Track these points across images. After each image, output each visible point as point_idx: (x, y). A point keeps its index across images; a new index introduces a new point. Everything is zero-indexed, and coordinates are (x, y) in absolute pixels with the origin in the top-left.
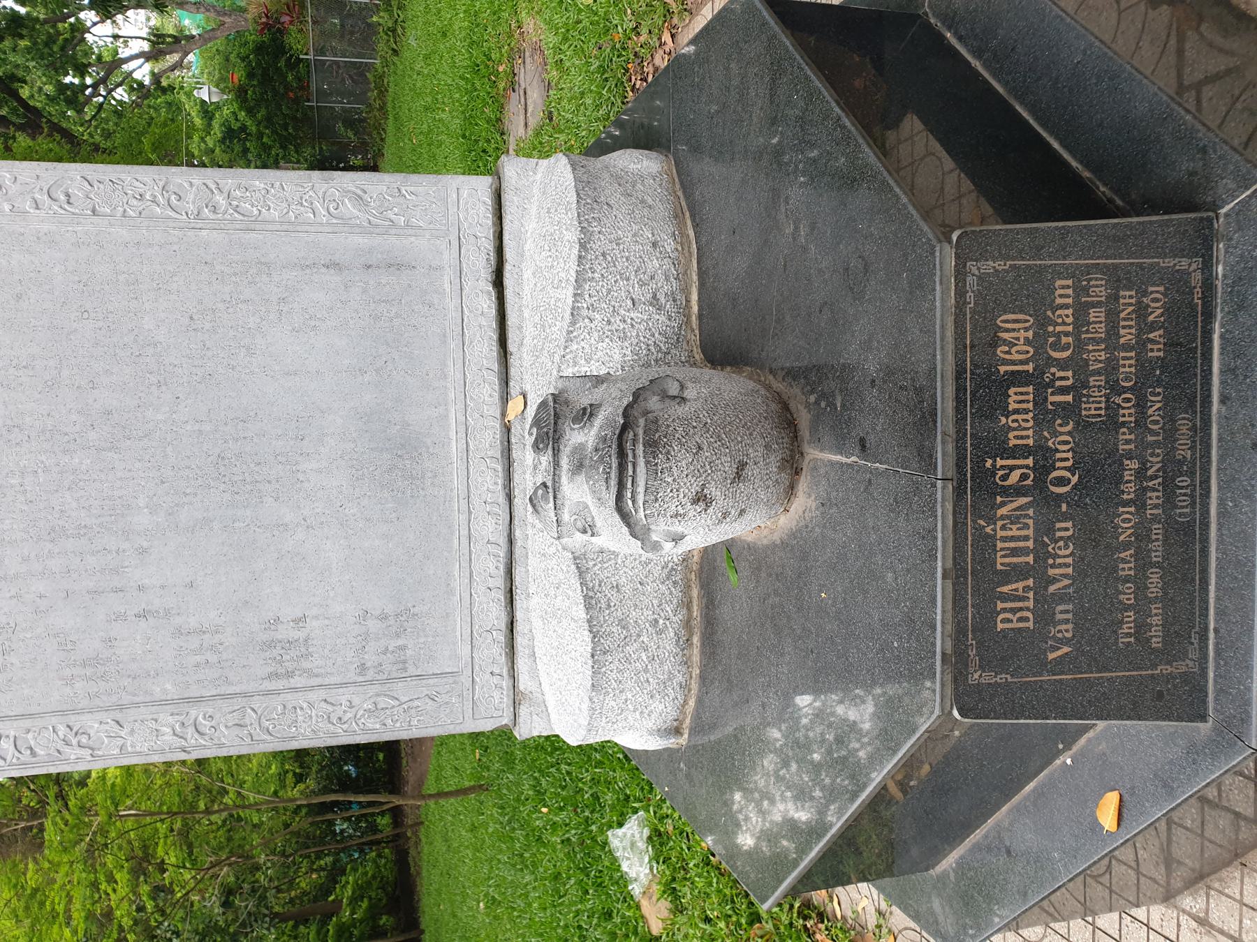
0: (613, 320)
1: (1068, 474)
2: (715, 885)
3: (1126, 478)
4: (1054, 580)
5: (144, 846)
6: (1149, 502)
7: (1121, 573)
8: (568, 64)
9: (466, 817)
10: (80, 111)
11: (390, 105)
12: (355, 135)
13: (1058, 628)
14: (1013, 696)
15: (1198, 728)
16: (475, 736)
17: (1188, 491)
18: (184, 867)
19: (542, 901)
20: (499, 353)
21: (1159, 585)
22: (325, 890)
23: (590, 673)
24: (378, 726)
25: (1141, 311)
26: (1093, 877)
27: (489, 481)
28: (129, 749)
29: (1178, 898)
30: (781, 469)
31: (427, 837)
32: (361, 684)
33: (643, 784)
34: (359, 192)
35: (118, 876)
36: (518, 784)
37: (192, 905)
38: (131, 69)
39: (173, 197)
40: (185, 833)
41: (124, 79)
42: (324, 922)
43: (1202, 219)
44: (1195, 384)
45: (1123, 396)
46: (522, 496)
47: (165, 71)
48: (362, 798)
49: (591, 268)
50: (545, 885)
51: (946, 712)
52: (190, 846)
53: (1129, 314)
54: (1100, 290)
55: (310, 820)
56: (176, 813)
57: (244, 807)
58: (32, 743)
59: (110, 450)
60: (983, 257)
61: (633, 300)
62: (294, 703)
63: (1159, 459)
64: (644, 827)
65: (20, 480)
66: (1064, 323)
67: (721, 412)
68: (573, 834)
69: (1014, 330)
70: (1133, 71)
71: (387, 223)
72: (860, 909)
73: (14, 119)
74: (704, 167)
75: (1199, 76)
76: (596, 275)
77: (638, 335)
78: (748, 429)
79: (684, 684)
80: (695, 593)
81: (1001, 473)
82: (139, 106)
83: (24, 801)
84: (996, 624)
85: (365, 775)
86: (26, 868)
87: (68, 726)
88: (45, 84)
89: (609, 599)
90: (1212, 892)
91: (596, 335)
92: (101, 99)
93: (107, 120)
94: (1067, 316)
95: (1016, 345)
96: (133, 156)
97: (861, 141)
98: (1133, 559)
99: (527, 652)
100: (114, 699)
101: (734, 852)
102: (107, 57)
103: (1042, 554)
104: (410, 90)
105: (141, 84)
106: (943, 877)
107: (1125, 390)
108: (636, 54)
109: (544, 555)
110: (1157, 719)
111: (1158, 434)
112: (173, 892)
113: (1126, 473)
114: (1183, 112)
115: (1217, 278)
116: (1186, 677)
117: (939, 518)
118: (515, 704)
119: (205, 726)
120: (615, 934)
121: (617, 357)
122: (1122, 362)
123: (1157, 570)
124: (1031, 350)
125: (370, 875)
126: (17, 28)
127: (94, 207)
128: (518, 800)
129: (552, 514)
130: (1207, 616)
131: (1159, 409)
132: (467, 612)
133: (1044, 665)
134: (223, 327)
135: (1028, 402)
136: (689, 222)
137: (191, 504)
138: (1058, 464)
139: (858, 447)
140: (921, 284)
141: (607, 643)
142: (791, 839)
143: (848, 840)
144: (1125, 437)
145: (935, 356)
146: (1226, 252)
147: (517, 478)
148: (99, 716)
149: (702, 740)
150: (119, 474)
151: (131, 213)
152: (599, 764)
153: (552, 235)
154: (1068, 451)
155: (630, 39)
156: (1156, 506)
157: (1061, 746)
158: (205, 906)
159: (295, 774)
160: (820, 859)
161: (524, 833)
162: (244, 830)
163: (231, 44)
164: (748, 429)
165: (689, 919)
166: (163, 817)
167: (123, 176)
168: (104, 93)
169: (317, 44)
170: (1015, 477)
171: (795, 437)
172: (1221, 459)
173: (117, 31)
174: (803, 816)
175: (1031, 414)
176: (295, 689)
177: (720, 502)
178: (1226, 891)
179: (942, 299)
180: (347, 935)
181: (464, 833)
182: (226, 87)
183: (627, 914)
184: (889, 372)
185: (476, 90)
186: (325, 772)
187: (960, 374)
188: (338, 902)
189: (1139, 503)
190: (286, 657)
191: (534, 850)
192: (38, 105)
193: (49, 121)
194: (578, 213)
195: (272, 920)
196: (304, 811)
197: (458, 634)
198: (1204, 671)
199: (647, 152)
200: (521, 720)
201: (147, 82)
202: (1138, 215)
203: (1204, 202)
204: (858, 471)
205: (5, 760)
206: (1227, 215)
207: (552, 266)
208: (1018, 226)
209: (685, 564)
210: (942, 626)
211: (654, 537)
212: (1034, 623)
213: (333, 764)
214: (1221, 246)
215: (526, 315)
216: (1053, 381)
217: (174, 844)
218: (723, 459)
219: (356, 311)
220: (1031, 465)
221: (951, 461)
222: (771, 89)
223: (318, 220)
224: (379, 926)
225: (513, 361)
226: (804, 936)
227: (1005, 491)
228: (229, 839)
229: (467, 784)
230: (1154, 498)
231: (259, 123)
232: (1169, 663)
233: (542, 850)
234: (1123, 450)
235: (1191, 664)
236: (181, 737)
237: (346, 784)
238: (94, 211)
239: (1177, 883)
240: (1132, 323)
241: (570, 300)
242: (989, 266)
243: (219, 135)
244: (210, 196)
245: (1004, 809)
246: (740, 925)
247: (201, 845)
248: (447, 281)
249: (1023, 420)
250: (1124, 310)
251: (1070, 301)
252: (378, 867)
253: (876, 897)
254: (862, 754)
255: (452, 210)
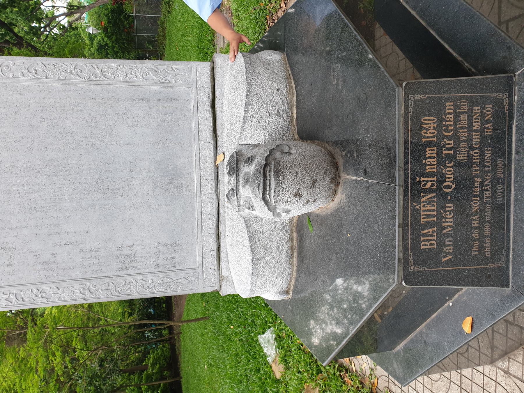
0: (261, 122)
1: (451, 184)
2: (303, 358)
3: (475, 186)
4: (445, 228)
5: (67, 342)
6: (485, 195)
7: (473, 225)
8: (241, 16)
9: (199, 330)
10: (39, 38)
11: (167, 35)
12: (153, 47)
13: (447, 248)
14: (427, 276)
15: (505, 290)
16: (203, 295)
17: (502, 191)
18: (84, 350)
19: (231, 365)
20: (213, 136)
21: (489, 230)
22: (141, 360)
23: (251, 268)
24: (164, 290)
25: (482, 115)
26: (461, 354)
27: (209, 189)
28: (62, 299)
29: (496, 362)
30: (331, 182)
31: (183, 339)
32: (157, 273)
33: (273, 316)
34: (155, 69)
35: (56, 354)
36: (221, 316)
37: (87, 366)
38: (60, 20)
39: (79, 71)
40: (84, 336)
41: (57, 25)
42: (141, 374)
43: (508, 77)
44: (505, 146)
45: (474, 151)
46: (223, 195)
47: (74, 21)
48: (156, 322)
49: (251, 100)
50: (232, 358)
51: (400, 283)
52: (86, 342)
53: (477, 117)
54: (465, 107)
55: (135, 331)
56: (80, 328)
57: (108, 325)
58: (23, 296)
59: (54, 176)
60: (416, 92)
61: (269, 113)
62: (129, 280)
63: (490, 177)
64: (273, 334)
65: (17, 188)
66: (450, 121)
67: (306, 159)
68: (244, 337)
69: (428, 124)
70: (480, 15)
71: (167, 82)
72: (363, 367)
73: (12, 41)
74: (299, 58)
75: (507, 18)
76: (254, 102)
77: (271, 128)
78: (317, 166)
79: (290, 273)
80: (295, 235)
81: (423, 183)
82: (63, 35)
83: (18, 323)
84: (421, 246)
85: (157, 313)
86: (19, 350)
87: (37, 289)
88: (24, 27)
89: (259, 237)
90: (511, 360)
91: (253, 128)
92: (47, 33)
93: (50, 41)
94: (451, 118)
95: (430, 130)
96: (61, 55)
97: (365, 45)
98: (478, 219)
99: (225, 260)
100: (56, 278)
101: (310, 345)
102: (50, 15)
103: (440, 217)
104: (176, 28)
105: (64, 27)
106: (398, 353)
107: (476, 148)
108: (270, 12)
109: (232, 219)
110: (488, 286)
111: (489, 167)
112: (79, 360)
113: (475, 183)
114: (500, 32)
115: (514, 102)
116: (500, 269)
117: (397, 202)
118: (220, 281)
119: (93, 290)
120: (261, 378)
121: (262, 137)
122: (474, 137)
123: (489, 224)
124: (436, 132)
125: (159, 354)
126: (12, 3)
127: (47, 75)
128: (221, 323)
129: (236, 201)
130: (509, 243)
131: (490, 156)
132: (200, 243)
133: (440, 264)
134: (100, 125)
135: (434, 153)
136: (292, 80)
137: (87, 198)
138: (447, 180)
139: (363, 173)
140: (389, 105)
141: (258, 256)
142: (334, 341)
143: (357, 339)
144: (475, 168)
145: (395, 134)
146: (519, 91)
147: (221, 188)
148: (50, 285)
149: (298, 296)
150: (57, 186)
151: (62, 78)
152: (255, 308)
153: (235, 86)
154: (451, 174)
155: (267, 5)
156: (488, 197)
157: (447, 298)
158: (92, 366)
159: (129, 313)
160: (347, 345)
161: (223, 337)
162: (108, 335)
163: (101, 9)
164: (317, 166)
165: (292, 372)
166: (75, 329)
167: (58, 62)
168: (48, 30)
169: (136, 9)
170: (429, 185)
171: (337, 169)
172: (516, 177)
173: (54, 4)
174: (339, 331)
175: (436, 159)
176: (130, 275)
177: (305, 196)
178: (517, 359)
179: (399, 111)
180: (150, 379)
181: (198, 337)
182: (99, 27)
183: (266, 370)
184: (376, 142)
185: (203, 28)
186: (141, 312)
187: (406, 142)
188: (147, 365)
189: (481, 196)
190: (126, 261)
191: (228, 344)
192: (22, 35)
193: (26, 42)
194: (246, 77)
195: (119, 372)
196: (132, 328)
197: (197, 252)
198: (508, 266)
199: (275, 51)
200: (223, 288)
201: (66, 25)
202: (481, 75)
203: (510, 70)
204: (363, 183)
205: (12, 303)
206: (519, 75)
207: (235, 99)
208: (431, 80)
209: (291, 223)
210: (398, 247)
211: (278, 211)
212: (437, 246)
213: (145, 308)
214: (516, 88)
215: (224, 120)
216: (445, 145)
217: (80, 341)
218: (307, 178)
219: (154, 118)
220: (436, 180)
221: (402, 178)
222: (327, 24)
223: (139, 80)
224: (164, 376)
225: (219, 139)
226: (340, 379)
227: (425, 191)
228: (102, 339)
229: (200, 317)
230: (487, 194)
231: (113, 42)
232: (493, 263)
233: (231, 344)
234: (474, 174)
235: (502, 263)
236: (83, 294)
237: (150, 317)
238: (46, 77)
239: (496, 356)
240: (479, 121)
241: (243, 113)
242: (418, 97)
243: (96, 48)
244: (94, 70)
245: (424, 324)
246: (313, 374)
247: (90, 342)
248: (192, 106)
249: (432, 161)
250: (475, 115)
251: (452, 111)
252: (163, 351)
253: (370, 363)
254: (364, 306)
255: (194, 76)
